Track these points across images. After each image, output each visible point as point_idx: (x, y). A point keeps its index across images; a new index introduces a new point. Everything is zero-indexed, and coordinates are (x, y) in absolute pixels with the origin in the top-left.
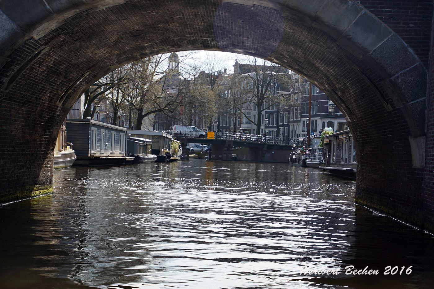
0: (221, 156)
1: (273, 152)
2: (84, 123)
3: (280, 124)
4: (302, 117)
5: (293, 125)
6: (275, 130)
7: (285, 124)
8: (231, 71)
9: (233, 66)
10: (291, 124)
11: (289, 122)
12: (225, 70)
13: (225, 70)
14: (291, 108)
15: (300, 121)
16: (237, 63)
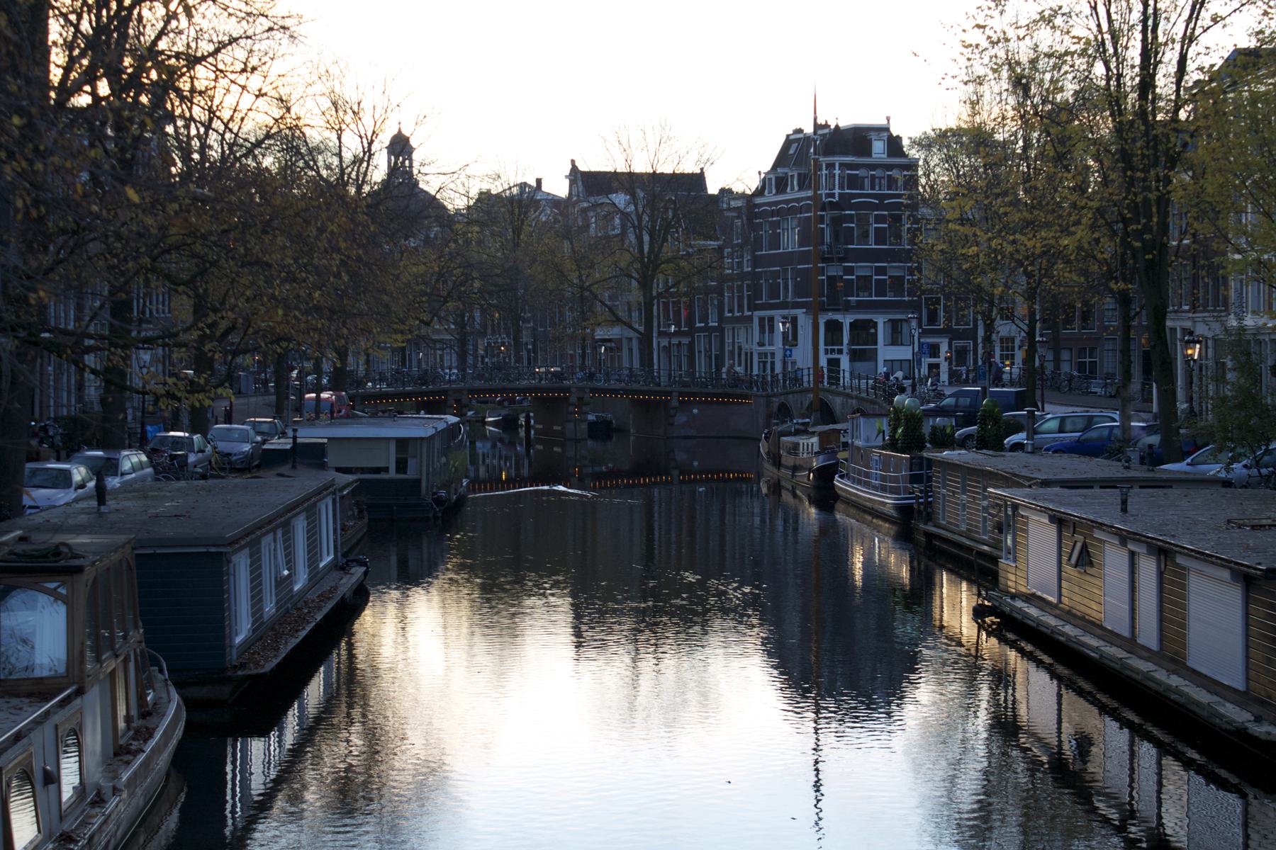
0: (559, 428)
1: (695, 411)
2: (204, 550)
3: (698, 325)
4: (752, 308)
5: (734, 328)
6: (685, 341)
7: (711, 324)
8: (558, 187)
9: (566, 177)
10: (727, 327)
11: (721, 319)
12: (539, 181)
13: (539, 181)
14: (617, 231)
15: (750, 318)
16: (574, 169)
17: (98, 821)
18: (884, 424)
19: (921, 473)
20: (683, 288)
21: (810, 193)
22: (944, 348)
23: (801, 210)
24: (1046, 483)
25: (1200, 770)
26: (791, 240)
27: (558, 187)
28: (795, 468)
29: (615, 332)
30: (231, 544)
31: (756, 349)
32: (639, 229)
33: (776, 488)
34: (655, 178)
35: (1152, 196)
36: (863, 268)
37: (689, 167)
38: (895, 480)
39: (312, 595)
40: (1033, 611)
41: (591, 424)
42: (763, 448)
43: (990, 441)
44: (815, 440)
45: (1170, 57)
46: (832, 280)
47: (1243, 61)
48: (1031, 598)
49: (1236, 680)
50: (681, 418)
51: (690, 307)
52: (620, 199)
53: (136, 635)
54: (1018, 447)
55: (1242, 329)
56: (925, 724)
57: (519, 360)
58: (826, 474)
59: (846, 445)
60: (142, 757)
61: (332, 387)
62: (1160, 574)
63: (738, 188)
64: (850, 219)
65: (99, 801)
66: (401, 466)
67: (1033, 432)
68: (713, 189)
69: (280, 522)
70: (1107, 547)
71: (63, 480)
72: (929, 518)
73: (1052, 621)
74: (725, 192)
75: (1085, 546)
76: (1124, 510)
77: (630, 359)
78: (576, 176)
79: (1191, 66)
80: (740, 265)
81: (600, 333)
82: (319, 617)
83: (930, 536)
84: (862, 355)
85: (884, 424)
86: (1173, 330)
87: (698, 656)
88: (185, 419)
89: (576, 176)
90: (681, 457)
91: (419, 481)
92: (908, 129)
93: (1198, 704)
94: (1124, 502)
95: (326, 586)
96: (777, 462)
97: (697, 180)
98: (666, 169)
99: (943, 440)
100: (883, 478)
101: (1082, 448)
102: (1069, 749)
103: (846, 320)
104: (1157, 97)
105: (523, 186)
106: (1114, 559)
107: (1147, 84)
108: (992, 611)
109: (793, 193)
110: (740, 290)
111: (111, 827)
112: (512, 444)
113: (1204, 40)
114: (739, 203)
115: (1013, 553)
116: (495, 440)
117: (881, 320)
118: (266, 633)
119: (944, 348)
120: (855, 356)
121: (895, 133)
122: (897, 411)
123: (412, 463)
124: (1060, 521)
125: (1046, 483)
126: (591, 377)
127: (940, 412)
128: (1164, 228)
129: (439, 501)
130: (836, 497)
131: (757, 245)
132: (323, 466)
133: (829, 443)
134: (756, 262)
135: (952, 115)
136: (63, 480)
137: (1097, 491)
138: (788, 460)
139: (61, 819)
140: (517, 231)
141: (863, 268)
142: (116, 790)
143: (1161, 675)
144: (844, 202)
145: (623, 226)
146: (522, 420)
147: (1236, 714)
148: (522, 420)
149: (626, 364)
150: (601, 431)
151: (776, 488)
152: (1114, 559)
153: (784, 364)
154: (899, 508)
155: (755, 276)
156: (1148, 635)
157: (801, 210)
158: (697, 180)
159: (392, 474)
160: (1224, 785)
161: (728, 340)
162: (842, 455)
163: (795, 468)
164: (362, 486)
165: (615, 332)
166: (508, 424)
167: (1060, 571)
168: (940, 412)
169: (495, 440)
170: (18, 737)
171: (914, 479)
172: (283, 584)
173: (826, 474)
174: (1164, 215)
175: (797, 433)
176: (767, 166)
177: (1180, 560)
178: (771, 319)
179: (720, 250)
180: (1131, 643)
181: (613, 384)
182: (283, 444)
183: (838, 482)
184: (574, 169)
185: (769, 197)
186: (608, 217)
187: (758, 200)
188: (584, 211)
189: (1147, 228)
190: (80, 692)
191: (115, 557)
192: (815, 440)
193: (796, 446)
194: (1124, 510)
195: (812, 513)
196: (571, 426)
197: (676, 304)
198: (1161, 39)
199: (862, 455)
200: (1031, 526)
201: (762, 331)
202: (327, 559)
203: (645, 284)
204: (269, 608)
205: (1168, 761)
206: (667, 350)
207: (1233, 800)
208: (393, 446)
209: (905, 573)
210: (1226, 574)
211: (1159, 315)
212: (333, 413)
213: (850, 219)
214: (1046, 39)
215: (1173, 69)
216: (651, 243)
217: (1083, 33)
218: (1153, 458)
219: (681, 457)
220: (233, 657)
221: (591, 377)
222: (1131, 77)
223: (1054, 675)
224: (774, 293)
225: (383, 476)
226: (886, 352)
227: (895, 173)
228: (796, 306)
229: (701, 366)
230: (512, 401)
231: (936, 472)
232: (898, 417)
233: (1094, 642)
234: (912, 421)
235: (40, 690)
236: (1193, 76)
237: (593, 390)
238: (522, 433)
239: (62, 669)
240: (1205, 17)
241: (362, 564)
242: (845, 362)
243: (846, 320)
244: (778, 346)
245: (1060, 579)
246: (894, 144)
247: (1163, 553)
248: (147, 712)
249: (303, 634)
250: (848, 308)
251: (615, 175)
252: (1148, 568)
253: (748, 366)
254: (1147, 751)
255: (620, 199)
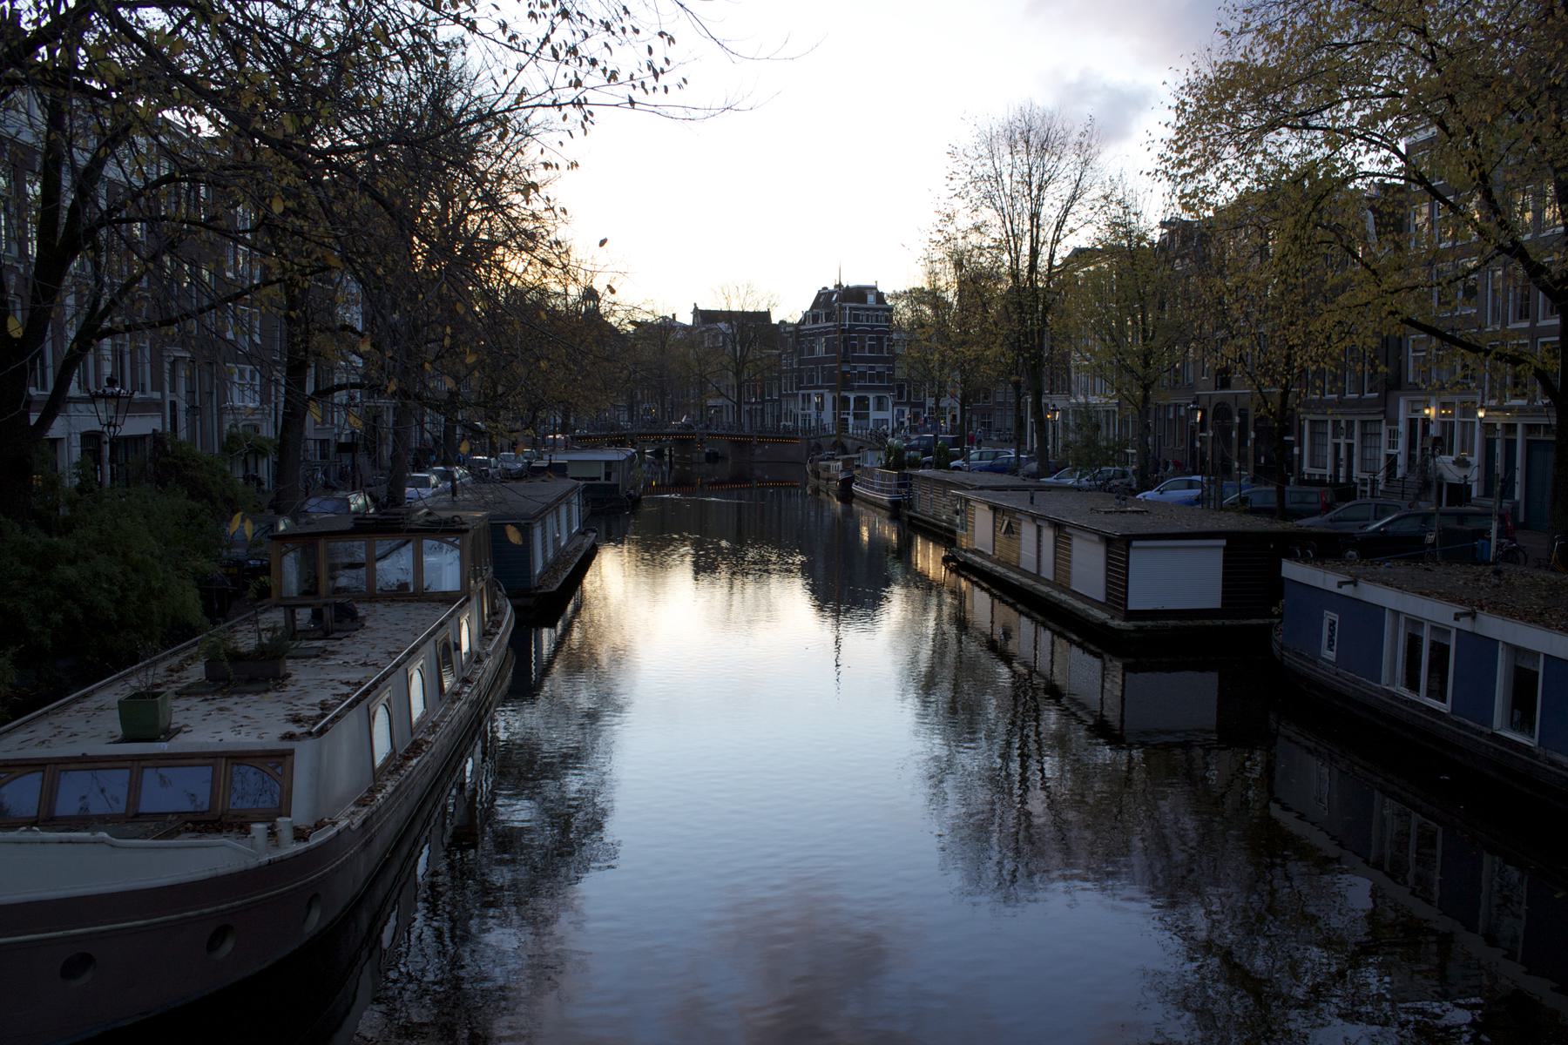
4: (799, 388)
6: (759, 407)
8: (686, 319)
11: (780, 395)
16: (696, 308)
17: (481, 671)
18: (882, 454)
19: (905, 482)
20: (758, 377)
21: (1525, 324)
22: (907, 412)
23: (827, 333)
24: (981, 488)
25: (1079, 645)
26: (820, 350)
27: (686, 319)
28: (828, 480)
29: (720, 401)
30: (534, 518)
31: (800, 412)
32: (734, 341)
33: (817, 491)
34: (744, 314)
35: (1036, 328)
36: (862, 367)
37: (763, 309)
38: (888, 486)
39: (570, 548)
40: (977, 559)
41: (707, 454)
42: (809, 468)
43: (942, 463)
44: (840, 463)
45: (1045, 252)
46: (845, 373)
47: (1079, 253)
48: (975, 552)
49: (1101, 597)
50: (758, 451)
51: (762, 388)
52: (723, 326)
53: (491, 570)
54: (957, 468)
55: (1087, 404)
56: (893, 627)
57: (663, 416)
58: (846, 484)
59: (858, 466)
60: (497, 637)
61: (562, 432)
62: (1056, 538)
63: (790, 320)
64: (855, 338)
65: (479, 661)
66: (608, 476)
67: (967, 460)
68: (775, 320)
69: (552, 507)
70: (1023, 523)
71: (425, 483)
72: (911, 507)
73: (989, 565)
74: (783, 322)
75: (1009, 524)
76: (1032, 503)
77: (728, 418)
78: (697, 313)
79: (1057, 256)
80: (791, 364)
81: (711, 402)
82: (576, 560)
83: (911, 518)
84: (861, 416)
85: (882, 454)
86: (1047, 405)
87: (766, 588)
88: (506, 448)
89: (697, 313)
90: (758, 472)
91: (617, 485)
92: (886, 288)
93: (1078, 609)
94: (1032, 498)
95: (576, 543)
96: (817, 476)
97: (767, 315)
98: (751, 309)
99: (916, 464)
100: (882, 485)
101: (991, 469)
102: (999, 631)
103: (852, 396)
104: (1037, 273)
105: (665, 318)
106: (1028, 531)
107: (1033, 267)
108: (953, 559)
109: (822, 324)
110: (791, 378)
111: (486, 675)
112: (660, 465)
113: (1064, 242)
114: (791, 329)
115: (964, 527)
116: (651, 463)
117: (871, 397)
118: (551, 568)
119: (907, 412)
120: (856, 416)
121: (880, 290)
122: (890, 447)
123: (614, 475)
124: (995, 509)
125: (981, 488)
126: (707, 427)
127: (910, 448)
128: (1041, 346)
129: (630, 496)
130: (853, 496)
131: (801, 352)
132: (565, 476)
133: (847, 465)
134: (800, 362)
135: (917, 279)
136: (425, 483)
137: (1009, 492)
138: (823, 474)
139: (463, 670)
140: (663, 343)
141: (862, 367)
142: (488, 655)
143: (1055, 594)
144: (852, 329)
145: (724, 341)
146: (667, 452)
147: (1101, 615)
148: (667, 452)
149: (724, 419)
150: (713, 458)
151: (817, 491)
152: (1028, 531)
153: (817, 421)
154: (891, 502)
155: (799, 370)
156: (1048, 573)
157: (827, 333)
158: (767, 315)
159: (603, 481)
160: (1091, 653)
161: (784, 407)
162: (856, 472)
163: (828, 480)
164: (587, 489)
165: (720, 401)
166: (659, 454)
167: (994, 535)
168: (910, 448)
169: (651, 463)
170: (442, 624)
171: (900, 485)
172: (556, 541)
173: (846, 484)
174: (1041, 338)
175: (828, 459)
176: (807, 307)
177: (1068, 530)
178: (809, 395)
179: (780, 355)
180: (1037, 577)
181: (720, 431)
182: (544, 463)
183: (854, 487)
184: (696, 308)
185: (809, 326)
186: (715, 337)
187: (802, 327)
188: (701, 332)
189: (1033, 346)
190: (468, 600)
191: (482, 524)
192: (840, 463)
193: (828, 467)
194: (1032, 503)
195: (838, 505)
196: (695, 455)
197: (755, 386)
198: (1041, 240)
199: (870, 472)
200: (977, 512)
201: (804, 402)
202: (575, 529)
203: (738, 374)
204: (550, 555)
205: (1058, 641)
206: (749, 412)
207: (1097, 663)
208: (603, 465)
209: (894, 537)
210: (1096, 538)
211: (1038, 395)
212: (567, 447)
213: (855, 338)
214: (974, 238)
215: (1047, 257)
216: (742, 350)
217: (998, 236)
218: (1036, 476)
219: (758, 472)
220: (535, 582)
221: (707, 427)
222: (1024, 262)
223: (991, 594)
224: (811, 380)
225: (597, 482)
226: (874, 415)
227: (880, 313)
228: (821, 387)
229: (768, 421)
230: (660, 441)
231: (914, 482)
232: (891, 450)
233: (1015, 576)
234: (899, 452)
235: (447, 598)
236: (1057, 262)
237: (709, 434)
238: (667, 459)
239: (458, 588)
240: (1065, 230)
241: (594, 531)
242: (851, 420)
243: (852, 396)
244: (813, 411)
245: (994, 540)
246: (880, 297)
247: (1058, 526)
248: (495, 612)
249: (570, 570)
250: (852, 389)
251: (721, 312)
252: (1048, 535)
253: (796, 421)
254: (1046, 636)
255: (723, 326)
